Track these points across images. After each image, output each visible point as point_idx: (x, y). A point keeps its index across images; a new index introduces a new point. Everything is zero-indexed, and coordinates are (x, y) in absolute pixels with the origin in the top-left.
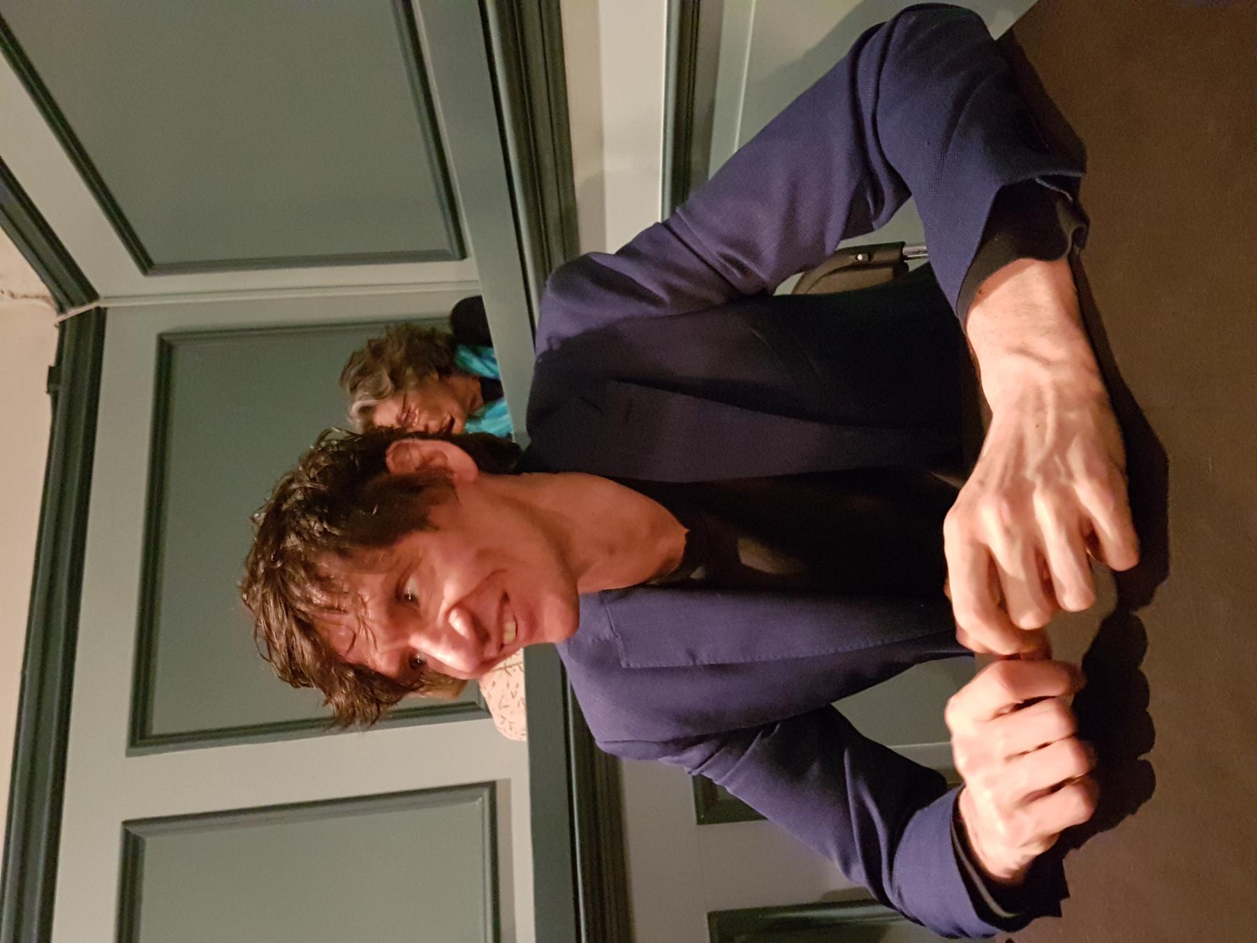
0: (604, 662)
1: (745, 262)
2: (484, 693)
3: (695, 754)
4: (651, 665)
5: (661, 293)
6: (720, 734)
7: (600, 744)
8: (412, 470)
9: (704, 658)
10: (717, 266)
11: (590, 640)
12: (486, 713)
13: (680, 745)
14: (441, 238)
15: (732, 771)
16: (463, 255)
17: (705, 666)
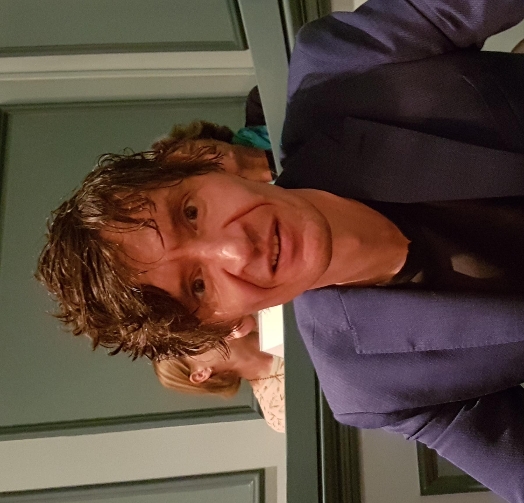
0: (341, 351)
1: (459, 16)
2: (257, 396)
3: (412, 424)
4: (379, 352)
5: (389, 44)
6: (430, 408)
7: (337, 418)
8: (224, 248)
9: (422, 346)
10: (435, 20)
11: (330, 332)
12: (261, 414)
13: (399, 416)
14: (229, 34)
15: (441, 437)
16: (246, 47)
17: (422, 353)
